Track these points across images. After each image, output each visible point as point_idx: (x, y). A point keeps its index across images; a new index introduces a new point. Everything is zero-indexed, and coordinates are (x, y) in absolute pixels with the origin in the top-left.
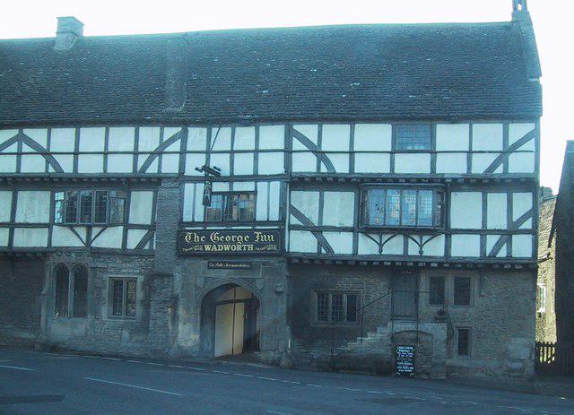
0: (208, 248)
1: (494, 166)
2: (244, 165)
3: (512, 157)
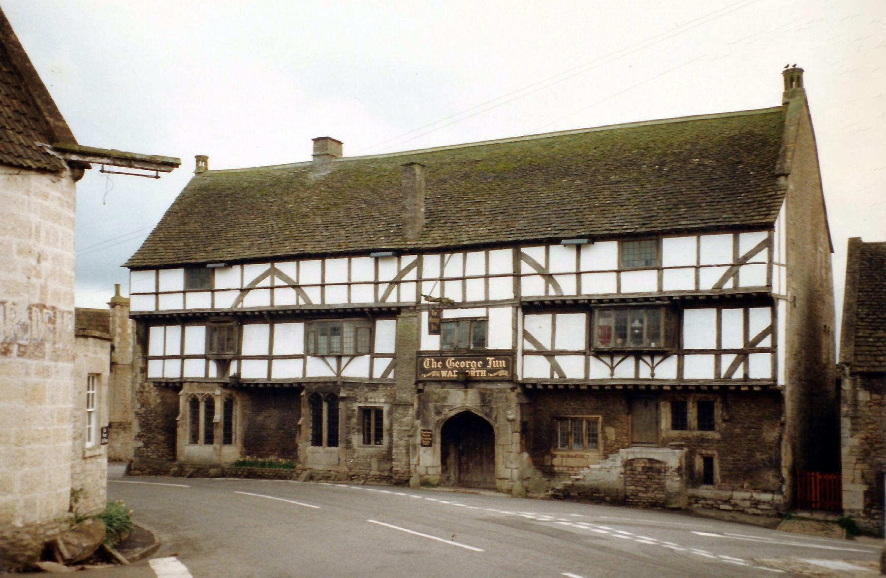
0: (444, 373)
1: (724, 279)
2: (476, 292)
3: (743, 270)
